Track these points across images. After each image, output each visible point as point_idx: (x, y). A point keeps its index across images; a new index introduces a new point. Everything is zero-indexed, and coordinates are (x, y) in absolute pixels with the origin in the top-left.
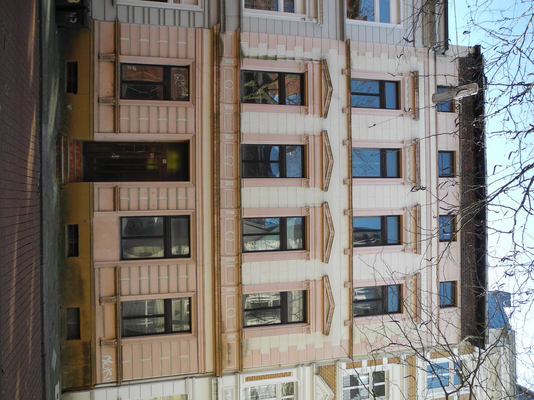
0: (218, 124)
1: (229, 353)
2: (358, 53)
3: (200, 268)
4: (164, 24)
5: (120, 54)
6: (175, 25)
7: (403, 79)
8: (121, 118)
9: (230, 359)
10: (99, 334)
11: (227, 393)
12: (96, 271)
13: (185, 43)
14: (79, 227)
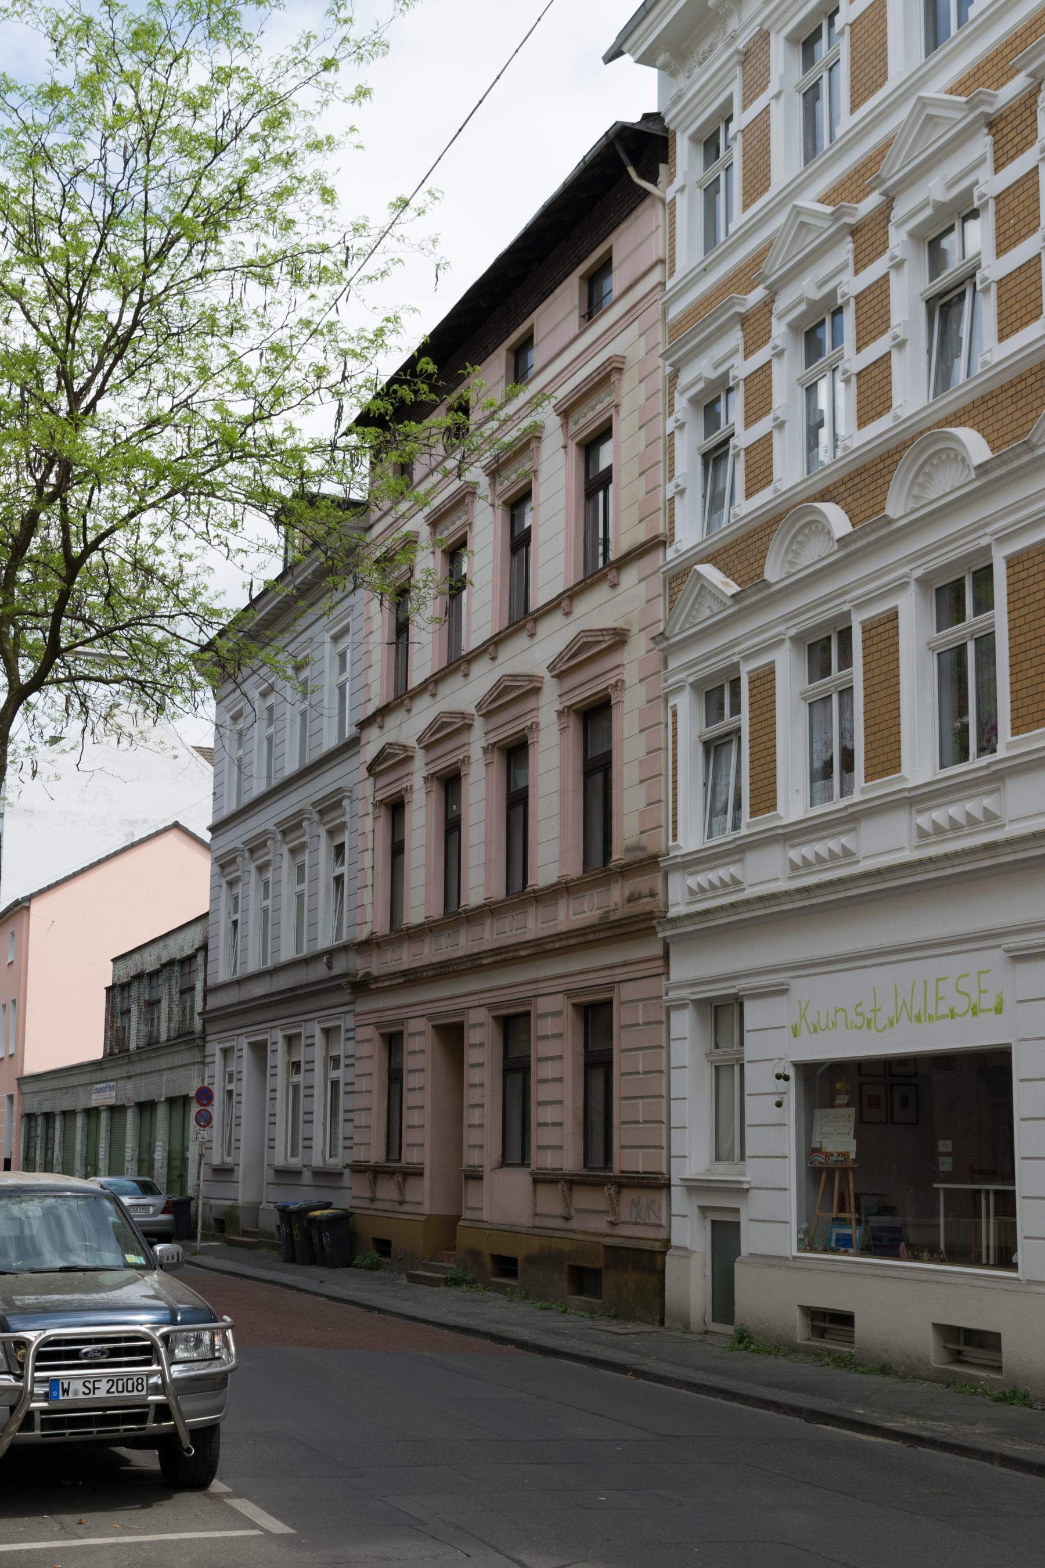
4: (353, 1084)
5: (561, 1169)
6: (353, 1065)
7: (500, 496)
10: (599, 1224)
11: (922, 833)
12: (538, 1222)
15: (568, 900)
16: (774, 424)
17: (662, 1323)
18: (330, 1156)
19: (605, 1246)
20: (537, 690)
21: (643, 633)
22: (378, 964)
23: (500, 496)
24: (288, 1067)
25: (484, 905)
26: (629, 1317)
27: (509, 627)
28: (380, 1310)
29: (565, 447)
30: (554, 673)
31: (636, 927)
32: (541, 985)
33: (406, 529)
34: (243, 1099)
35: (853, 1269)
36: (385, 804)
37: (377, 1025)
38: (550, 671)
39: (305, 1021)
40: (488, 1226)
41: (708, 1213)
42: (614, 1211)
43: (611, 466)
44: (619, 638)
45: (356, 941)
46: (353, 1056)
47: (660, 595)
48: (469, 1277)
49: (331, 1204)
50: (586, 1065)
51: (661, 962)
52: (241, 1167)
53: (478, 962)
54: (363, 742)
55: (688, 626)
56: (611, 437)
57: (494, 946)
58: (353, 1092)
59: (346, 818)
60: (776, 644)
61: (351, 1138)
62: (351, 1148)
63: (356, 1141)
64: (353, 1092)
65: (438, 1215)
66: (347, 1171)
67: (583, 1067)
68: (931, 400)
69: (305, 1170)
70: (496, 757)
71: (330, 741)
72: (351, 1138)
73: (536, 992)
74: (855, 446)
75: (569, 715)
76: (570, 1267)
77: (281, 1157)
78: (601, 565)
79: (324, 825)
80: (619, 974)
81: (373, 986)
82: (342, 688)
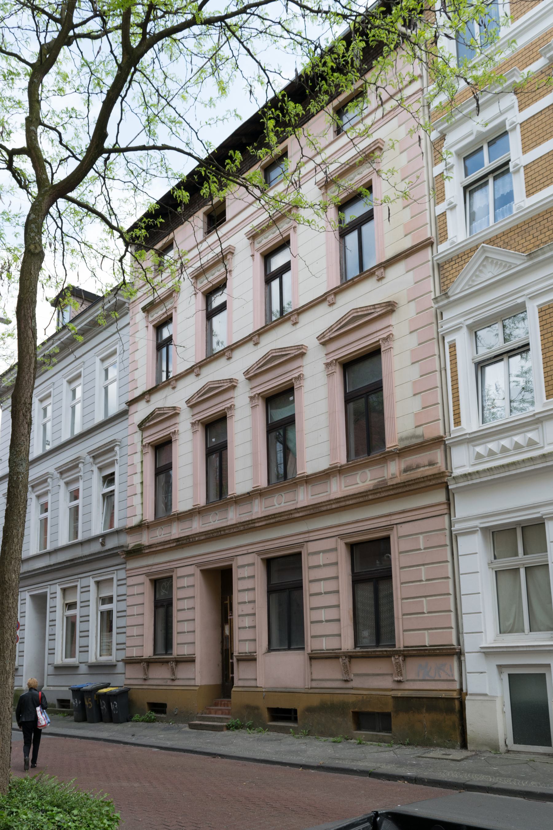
0: (369, 493)
1: (418, 467)
2: (136, 388)
3: (313, 536)
4: (125, 611)
5: (341, 649)
6: (125, 600)
7: (258, 250)
8: (324, 648)
9: (426, 463)
10: (387, 683)
11: (479, 456)
12: (314, 684)
13: (321, 554)
14: (280, 707)
15: (261, 502)
16: (447, 207)
17: (464, 745)
18: (100, 656)
19: (393, 697)
20: (177, 414)
21: (413, 304)
22: (145, 539)
23: (258, 250)
24: (63, 606)
25: (192, 509)
26: (426, 743)
27: (341, 285)
28: (223, 756)
29: (253, 256)
30: (189, 405)
31: (423, 485)
32: (311, 534)
33: (375, 136)
34: (26, 627)
35: (243, 690)
36: (152, 446)
37: (198, 565)
38: (187, 404)
39: (80, 578)
40: (264, 690)
41: (504, 670)
42: (400, 673)
43: (226, 301)
44: (232, 385)
45: (127, 527)
46: (125, 595)
47: (430, 276)
48: (250, 723)
49: (109, 684)
50: (353, 581)
51: (445, 506)
52: (24, 667)
53: (253, 525)
54: (130, 413)
55: (467, 288)
56: (226, 287)
57: (263, 515)
58: (125, 616)
59: (117, 457)
60: (458, 329)
61: (125, 644)
62: (125, 649)
63: (127, 645)
64: (125, 616)
65: (205, 685)
66: (121, 664)
67: (351, 583)
68: (468, 237)
69: (81, 665)
70: (200, 430)
71: (114, 410)
72: (125, 644)
73: (307, 539)
74: (527, 206)
75: (198, 425)
76: (353, 712)
77: (60, 658)
78: (164, 379)
79: (96, 464)
80: (395, 519)
81: (147, 551)
82: (45, 426)
